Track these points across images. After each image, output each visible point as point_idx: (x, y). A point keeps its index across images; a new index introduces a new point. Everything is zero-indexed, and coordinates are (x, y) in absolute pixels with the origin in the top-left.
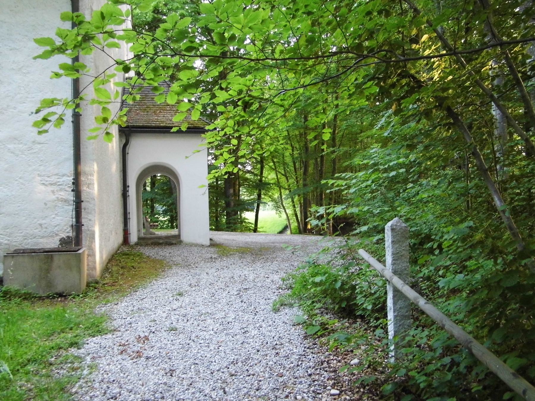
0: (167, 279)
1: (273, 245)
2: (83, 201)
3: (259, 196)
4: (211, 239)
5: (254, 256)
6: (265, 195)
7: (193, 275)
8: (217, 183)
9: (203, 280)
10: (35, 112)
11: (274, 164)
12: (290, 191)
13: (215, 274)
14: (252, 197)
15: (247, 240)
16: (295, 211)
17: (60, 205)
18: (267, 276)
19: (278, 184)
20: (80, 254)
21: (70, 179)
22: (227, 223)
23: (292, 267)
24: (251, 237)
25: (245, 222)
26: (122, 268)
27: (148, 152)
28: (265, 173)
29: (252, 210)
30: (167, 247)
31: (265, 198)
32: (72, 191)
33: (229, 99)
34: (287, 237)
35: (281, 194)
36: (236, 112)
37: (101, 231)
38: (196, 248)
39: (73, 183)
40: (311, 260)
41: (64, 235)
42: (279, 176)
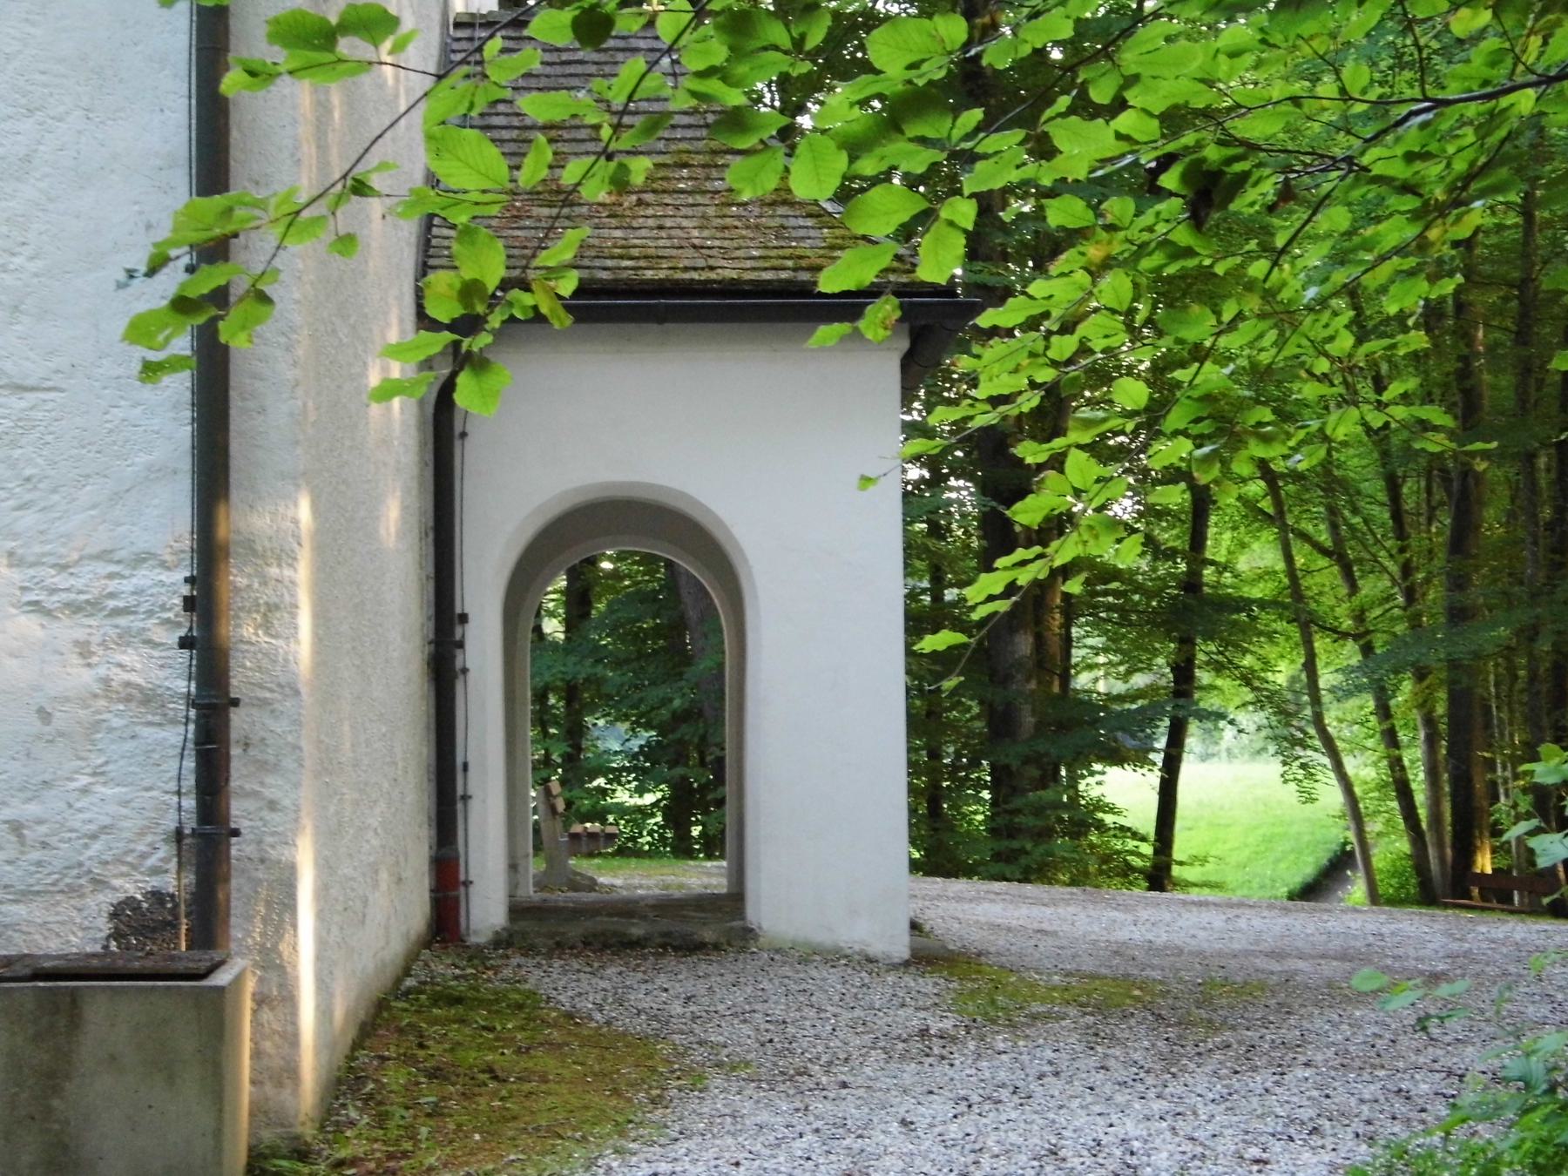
0: (681, 1148)
1: (1277, 967)
2: (235, 703)
3: (1184, 674)
4: (915, 926)
5: (1172, 1033)
6: (1218, 668)
7: (827, 1131)
8: (937, 597)
9: (888, 1161)
10: (143, 269)
11: (1273, 489)
12: (1367, 650)
13: (954, 1131)
14: (1140, 680)
15: (1122, 935)
16: (1396, 764)
17: (116, 722)
18: (1254, 1152)
19: (1297, 608)
20: (220, 990)
21: (174, 581)
22: (994, 832)
23: (1399, 1106)
24: (1144, 914)
25: (1101, 826)
26: (435, 1074)
27: (594, 427)
28: (1219, 542)
29: (1139, 758)
30: (670, 961)
31: (1218, 690)
32: (185, 643)
33: (1111, 160)
34: (1354, 923)
35: (1310, 667)
36: (1150, 229)
37: (325, 866)
38: (833, 977)
39: (189, 604)
40: (1536, 1065)
41: (131, 887)
42: (1300, 561)
